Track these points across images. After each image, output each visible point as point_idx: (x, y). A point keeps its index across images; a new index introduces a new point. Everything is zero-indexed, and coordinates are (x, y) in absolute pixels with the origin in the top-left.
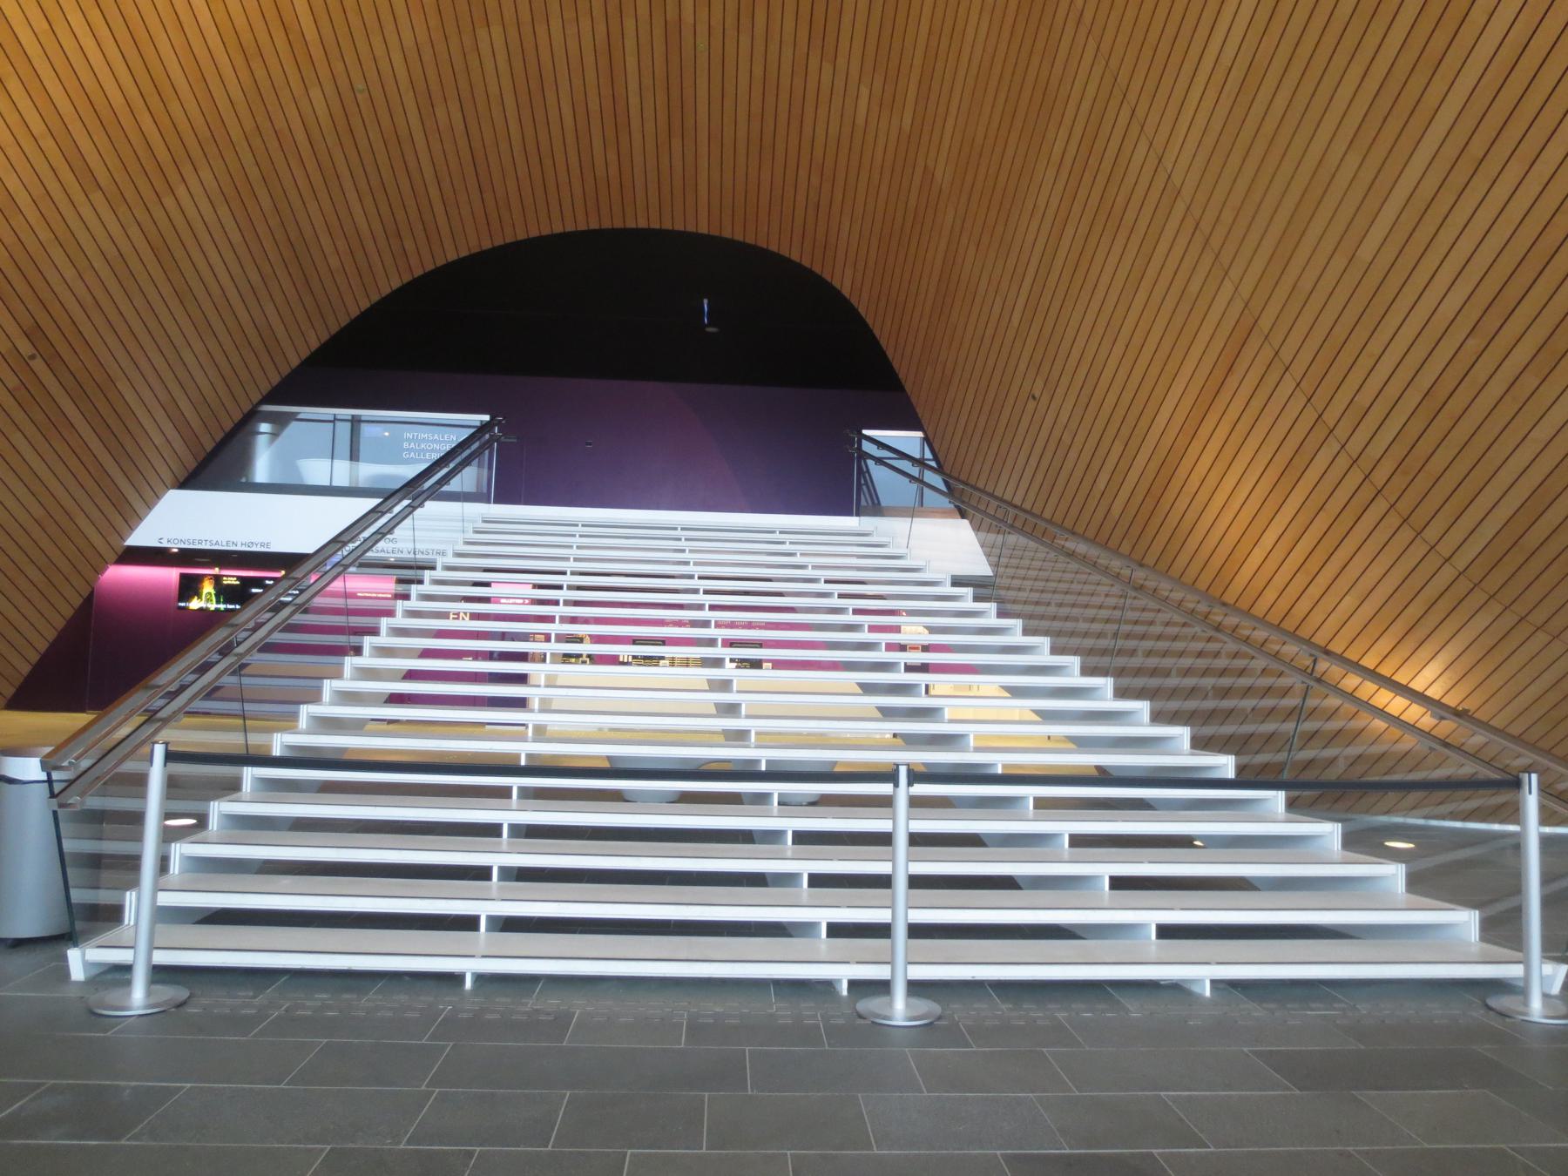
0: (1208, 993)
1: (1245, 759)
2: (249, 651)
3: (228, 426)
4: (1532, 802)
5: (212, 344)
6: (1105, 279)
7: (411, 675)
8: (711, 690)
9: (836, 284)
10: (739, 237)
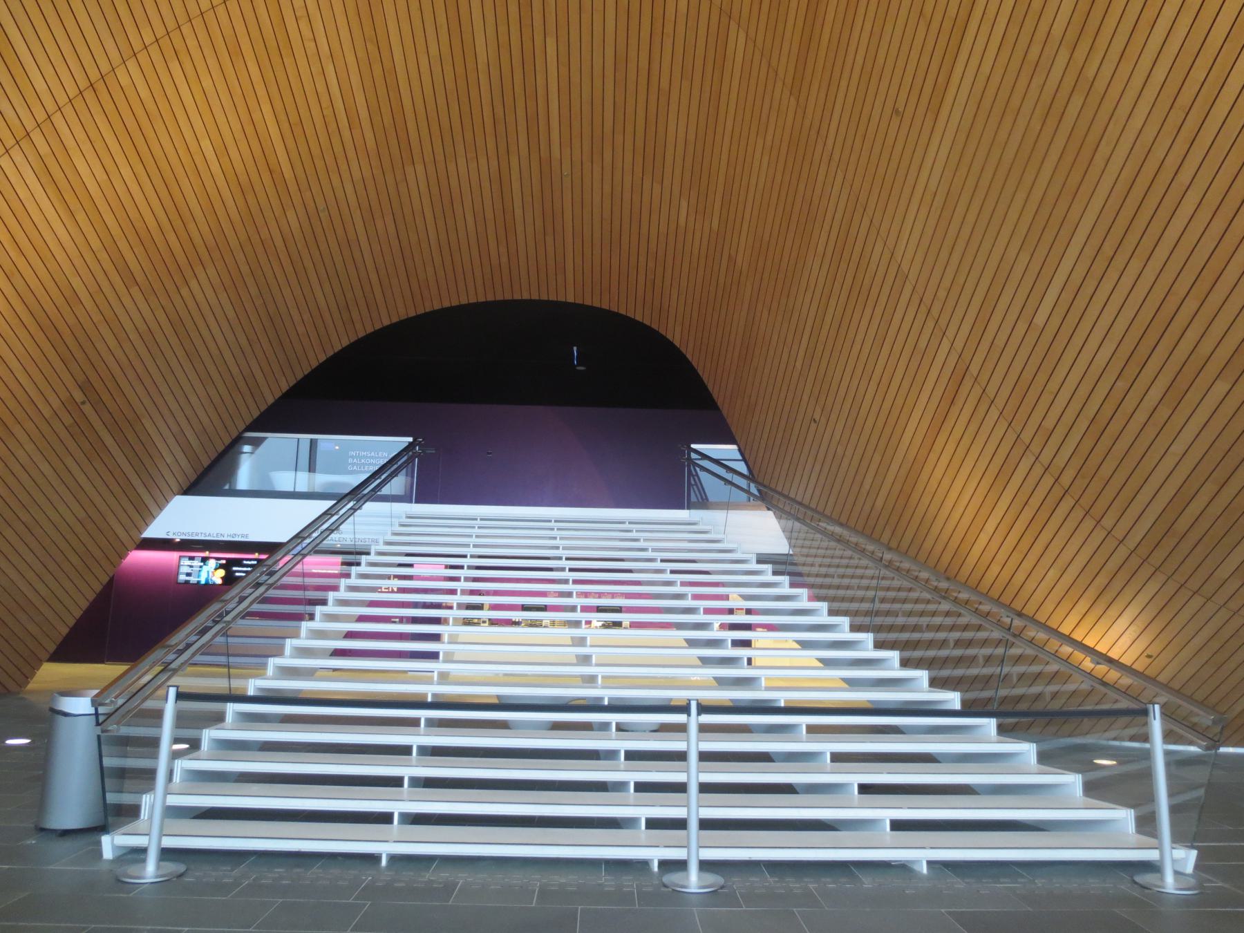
0: (925, 871)
1: (972, 695)
2: (234, 618)
3: (221, 448)
4: (1156, 726)
5: (213, 392)
8: (573, 645)
9: (669, 337)
10: (597, 304)
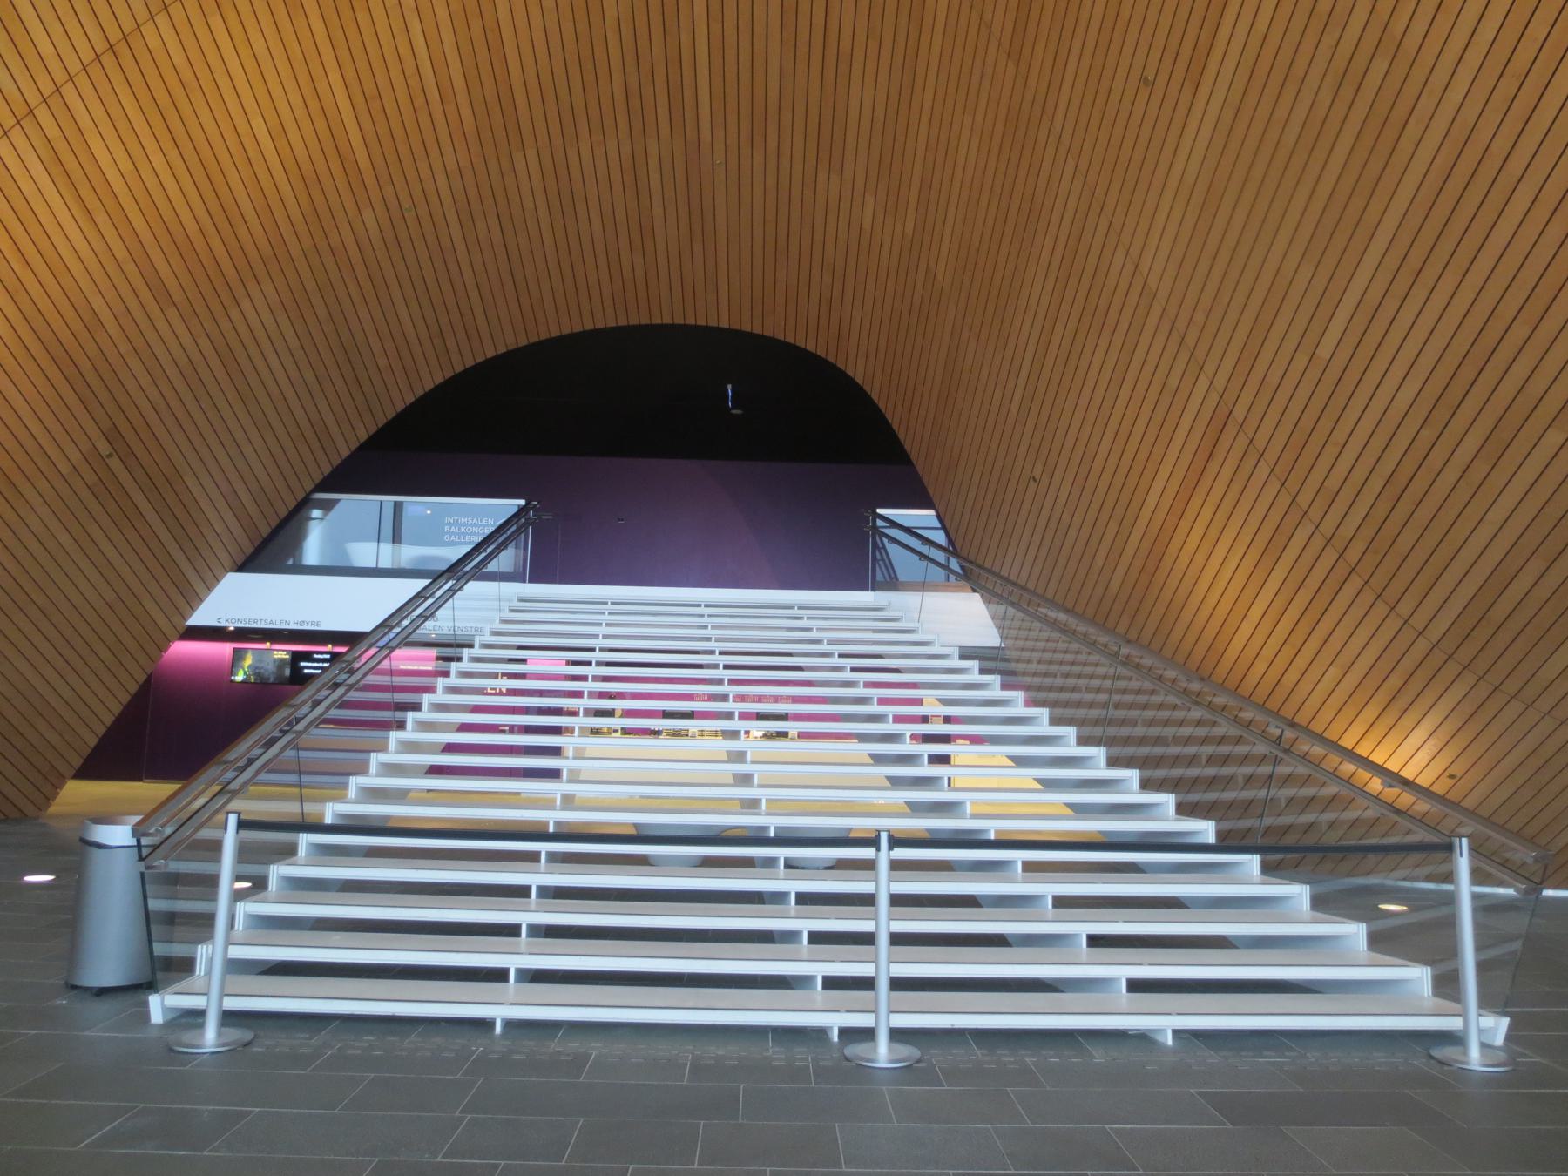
0: (1170, 1042)
1: (1227, 825)
3: (283, 513)
4: (1463, 864)
6: (1093, 373)
7: (450, 748)
9: (850, 372)
10: (757, 330)
